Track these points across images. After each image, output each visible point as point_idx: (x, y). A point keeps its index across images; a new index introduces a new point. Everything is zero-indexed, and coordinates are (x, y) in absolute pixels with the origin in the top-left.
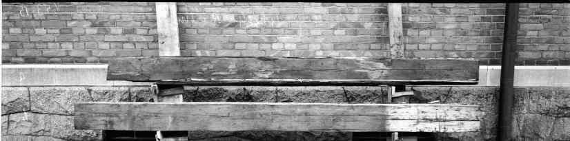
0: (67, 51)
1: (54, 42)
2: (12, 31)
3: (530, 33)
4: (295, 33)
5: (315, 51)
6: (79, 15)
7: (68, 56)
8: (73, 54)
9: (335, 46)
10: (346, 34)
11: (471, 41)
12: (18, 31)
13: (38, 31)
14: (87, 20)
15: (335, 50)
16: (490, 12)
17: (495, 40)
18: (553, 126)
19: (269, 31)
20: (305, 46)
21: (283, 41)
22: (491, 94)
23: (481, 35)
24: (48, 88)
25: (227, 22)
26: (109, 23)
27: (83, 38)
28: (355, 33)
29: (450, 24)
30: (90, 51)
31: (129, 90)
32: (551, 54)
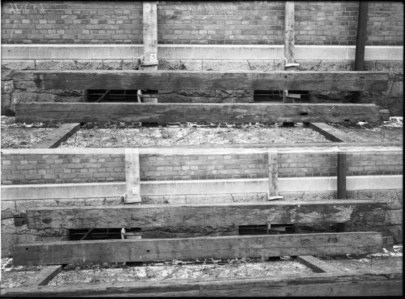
0: (41, 175)
1: (33, 169)
2: (24, 21)
3: (375, 23)
4: (215, 23)
5: (229, 36)
6: (68, 11)
7: (61, 38)
8: (65, 37)
9: (242, 32)
10: (250, 24)
11: (316, 161)
12: (28, 21)
13: (41, 22)
14: (74, 14)
15: (224, 169)
16: (348, 9)
17: (352, 28)
18: (392, 87)
19: (180, 158)
20: (205, 167)
21: (189, 164)
22: (332, 195)
23: (343, 25)
24: (29, 201)
25: (169, 16)
26: (89, 16)
27: (71, 26)
28: (256, 23)
29: (321, 17)
30: (58, 175)
31: (85, 201)
32: (390, 38)
